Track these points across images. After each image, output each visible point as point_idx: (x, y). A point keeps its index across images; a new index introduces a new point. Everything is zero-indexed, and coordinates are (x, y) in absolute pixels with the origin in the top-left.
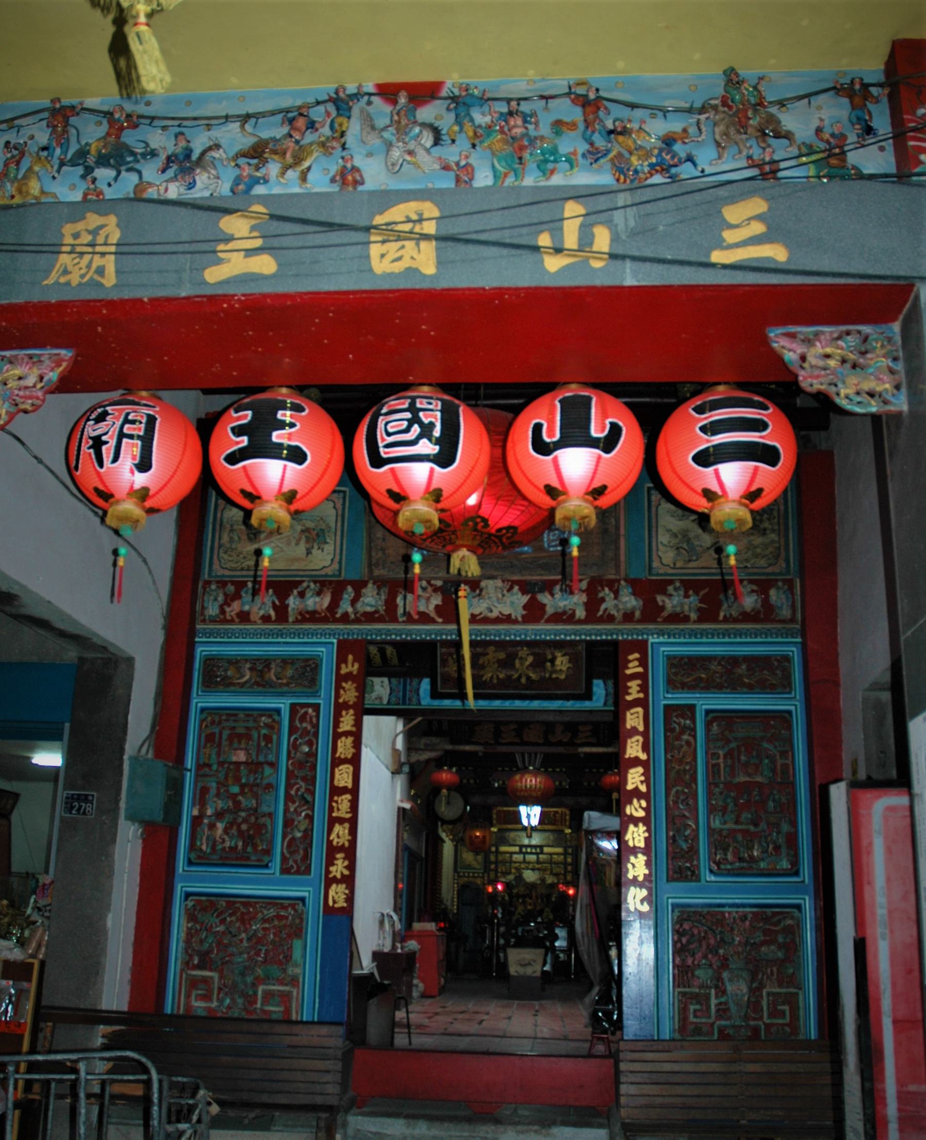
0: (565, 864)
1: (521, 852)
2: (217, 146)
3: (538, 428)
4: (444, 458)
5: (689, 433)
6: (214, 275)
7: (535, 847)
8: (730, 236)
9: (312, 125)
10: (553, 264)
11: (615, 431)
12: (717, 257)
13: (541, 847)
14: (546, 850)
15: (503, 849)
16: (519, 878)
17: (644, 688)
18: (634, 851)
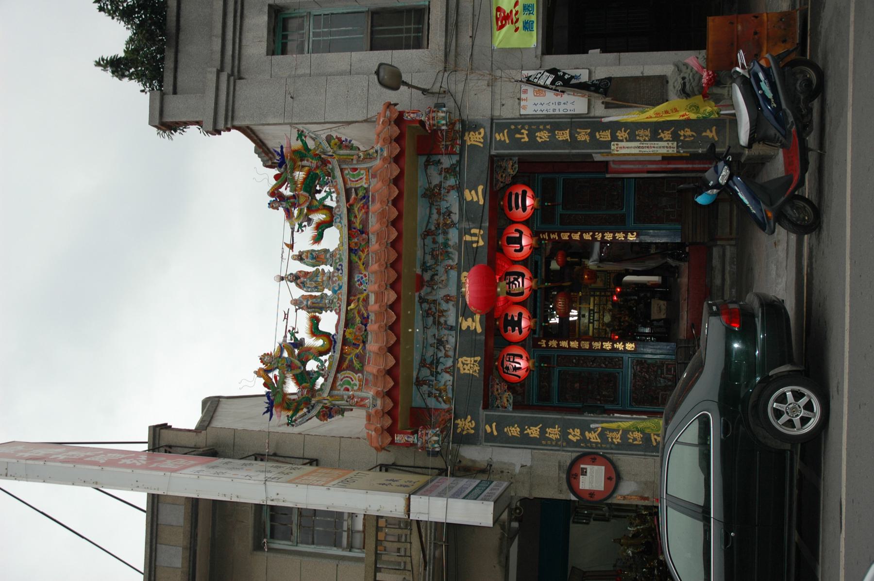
0: (600, 296)
1: (593, 323)
2: (434, 335)
3: (516, 251)
4: (523, 275)
5: (519, 213)
6: (479, 330)
7: (590, 314)
8: (475, 199)
9: (430, 309)
10: (481, 243)
11: (517, 230)
12: (481, 202)
13: (590, 310)
14: (592, 308)
15: (591, 333)
16: (608, 325)
17: (554, 233)
18: (614, 237)
